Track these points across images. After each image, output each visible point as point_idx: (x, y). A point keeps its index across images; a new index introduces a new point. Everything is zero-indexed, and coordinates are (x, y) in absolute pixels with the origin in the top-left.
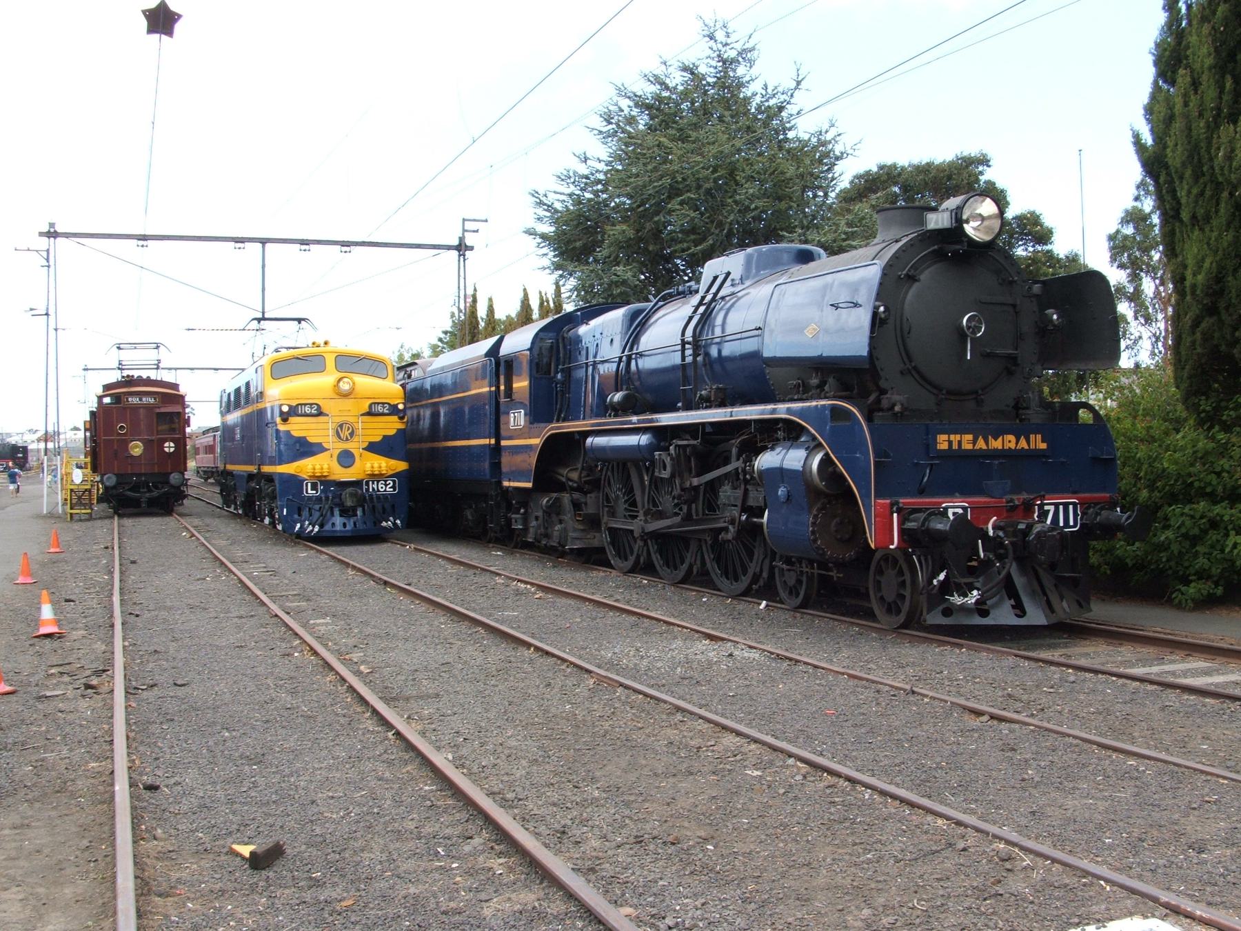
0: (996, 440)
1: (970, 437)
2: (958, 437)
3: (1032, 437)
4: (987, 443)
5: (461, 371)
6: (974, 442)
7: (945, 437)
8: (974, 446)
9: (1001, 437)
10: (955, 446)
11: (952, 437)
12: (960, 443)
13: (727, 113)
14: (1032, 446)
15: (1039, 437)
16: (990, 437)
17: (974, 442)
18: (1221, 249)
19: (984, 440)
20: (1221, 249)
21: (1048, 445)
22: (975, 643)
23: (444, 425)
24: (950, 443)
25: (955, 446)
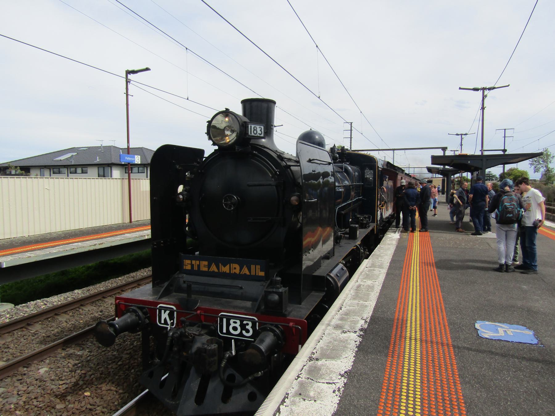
0: (225, 267)
1: (206, 263)
2: (198, 262)
3: (253, 267)
4: (218, 268)
5: (464, 383)
6: (209, 266)
7: (189, 262)
8: (209, 269)
9: (229, 265)
10: (196, 268)
11: (194, 262)
12: (199, 266)
13: (34, 345)
14: (253, 273)
15: (258, 267)
16: (220, 264)
17: (209, 266)
18: (95, 407)
19: (216, 266)
20: (95, 407)
21: (265, 274)
22: (312, 310)
23: (304, 270)
24: (192, 266)
25: (196, 268)
